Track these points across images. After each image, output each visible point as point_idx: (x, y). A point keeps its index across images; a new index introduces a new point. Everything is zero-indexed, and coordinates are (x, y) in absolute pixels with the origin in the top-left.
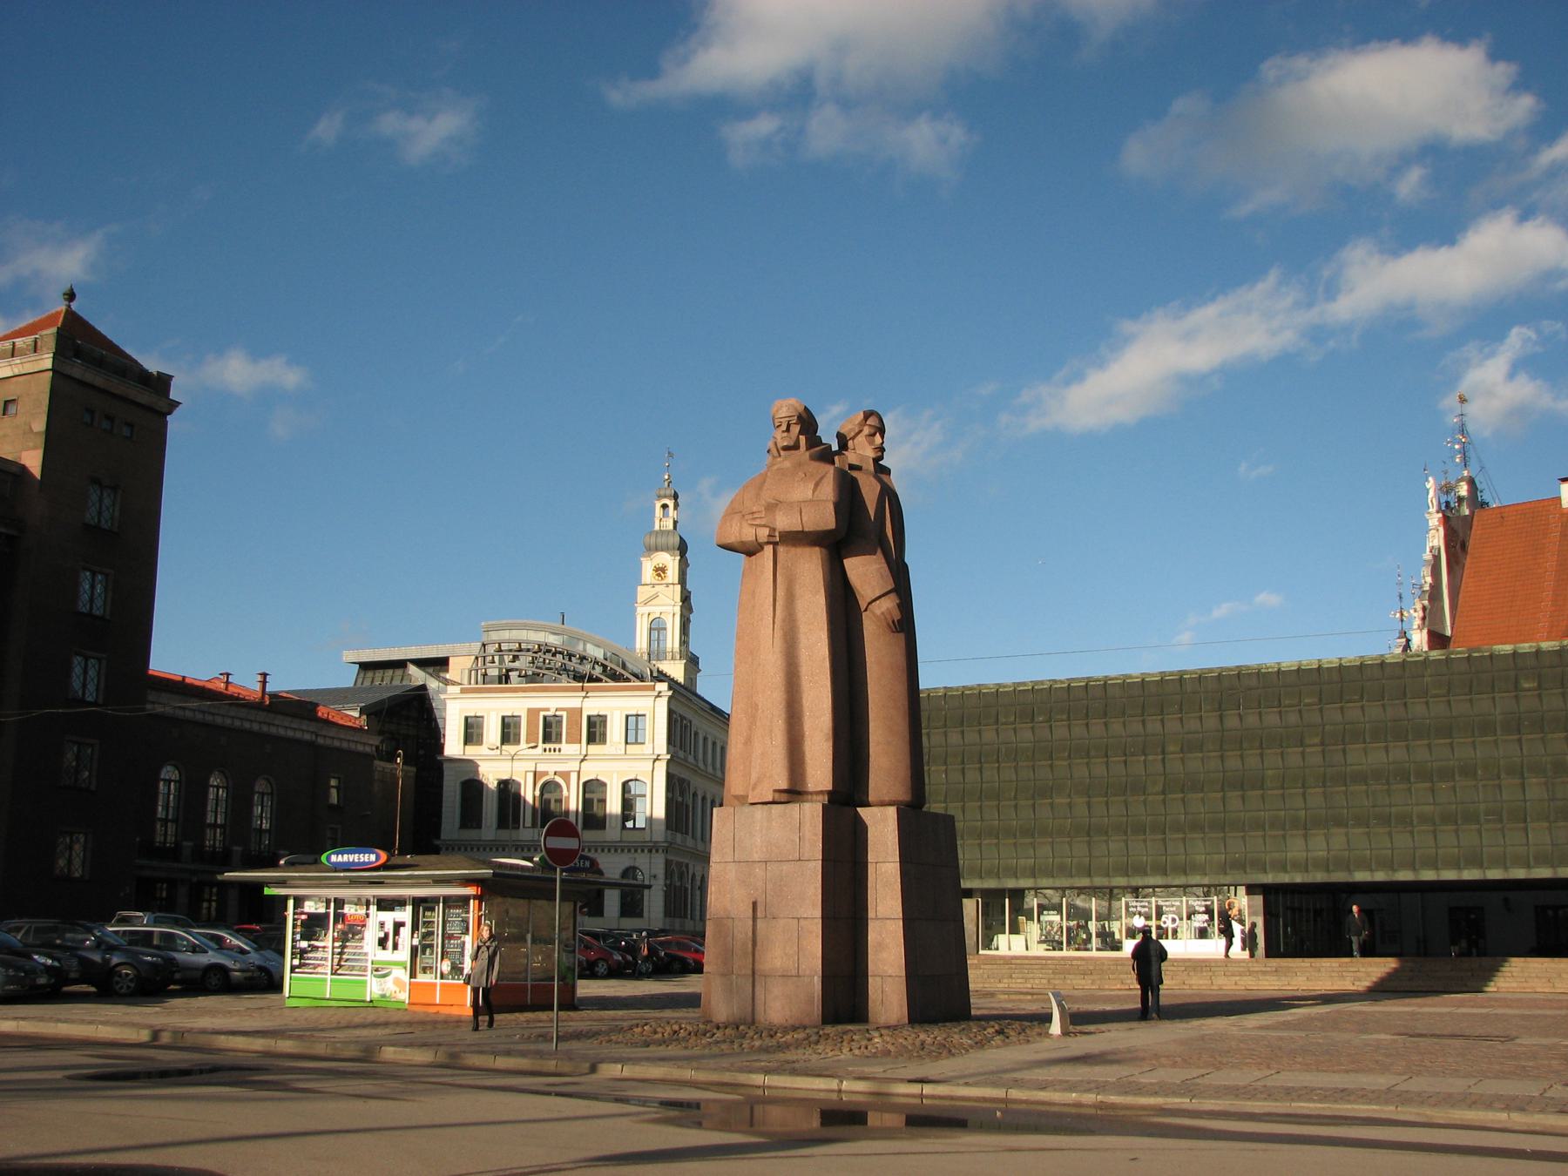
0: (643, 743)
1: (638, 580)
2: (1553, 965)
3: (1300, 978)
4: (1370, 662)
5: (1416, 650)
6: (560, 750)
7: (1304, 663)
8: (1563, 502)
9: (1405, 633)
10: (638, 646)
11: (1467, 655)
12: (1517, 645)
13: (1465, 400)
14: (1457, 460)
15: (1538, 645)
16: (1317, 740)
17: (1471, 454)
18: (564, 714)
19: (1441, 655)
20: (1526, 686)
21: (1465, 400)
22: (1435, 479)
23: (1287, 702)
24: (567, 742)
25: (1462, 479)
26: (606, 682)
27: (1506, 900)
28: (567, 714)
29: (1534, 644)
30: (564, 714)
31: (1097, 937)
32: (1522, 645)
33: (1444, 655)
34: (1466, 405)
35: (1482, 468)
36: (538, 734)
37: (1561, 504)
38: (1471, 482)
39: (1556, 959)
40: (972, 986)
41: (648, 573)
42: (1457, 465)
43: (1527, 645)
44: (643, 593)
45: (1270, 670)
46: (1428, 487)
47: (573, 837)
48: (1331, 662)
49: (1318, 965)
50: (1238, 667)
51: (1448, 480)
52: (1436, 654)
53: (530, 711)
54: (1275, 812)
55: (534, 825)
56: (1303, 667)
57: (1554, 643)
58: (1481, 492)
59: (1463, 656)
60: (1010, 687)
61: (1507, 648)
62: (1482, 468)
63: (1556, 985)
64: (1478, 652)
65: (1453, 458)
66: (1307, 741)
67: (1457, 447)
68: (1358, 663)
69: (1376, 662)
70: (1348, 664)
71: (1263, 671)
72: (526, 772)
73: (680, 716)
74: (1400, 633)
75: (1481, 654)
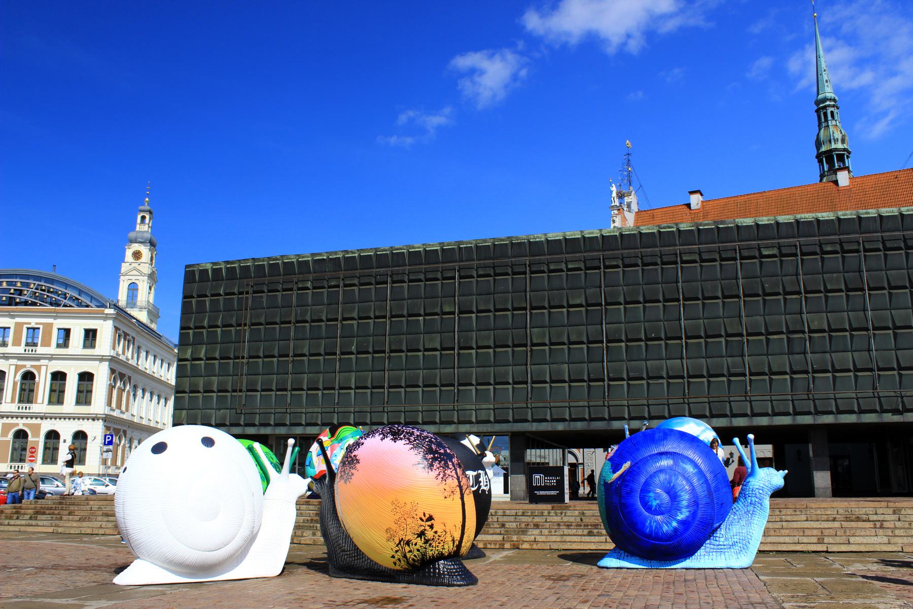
0: (59, 329)
1: (122, 259)
6: (36, 351)
17: (634, 178)
18: (41, 327)
22: (615, 185)
28: (43, 327)
29: (772, 218)
30: (41, 327)
31: (37, 343)
36: (21, 340)
40: (816, 486)
41: (129, 254)
43: (765, 218)
44: (125, 267)
45: (537, 240)
46: (612, 190)
50: (508, 237)
53: (17, 324)
55: (13, 401)
57: (788, 217)
60: (308, 257)
70: (608, 234)
72: (10, 365)
73: (123, 332)
75: (726, 226)
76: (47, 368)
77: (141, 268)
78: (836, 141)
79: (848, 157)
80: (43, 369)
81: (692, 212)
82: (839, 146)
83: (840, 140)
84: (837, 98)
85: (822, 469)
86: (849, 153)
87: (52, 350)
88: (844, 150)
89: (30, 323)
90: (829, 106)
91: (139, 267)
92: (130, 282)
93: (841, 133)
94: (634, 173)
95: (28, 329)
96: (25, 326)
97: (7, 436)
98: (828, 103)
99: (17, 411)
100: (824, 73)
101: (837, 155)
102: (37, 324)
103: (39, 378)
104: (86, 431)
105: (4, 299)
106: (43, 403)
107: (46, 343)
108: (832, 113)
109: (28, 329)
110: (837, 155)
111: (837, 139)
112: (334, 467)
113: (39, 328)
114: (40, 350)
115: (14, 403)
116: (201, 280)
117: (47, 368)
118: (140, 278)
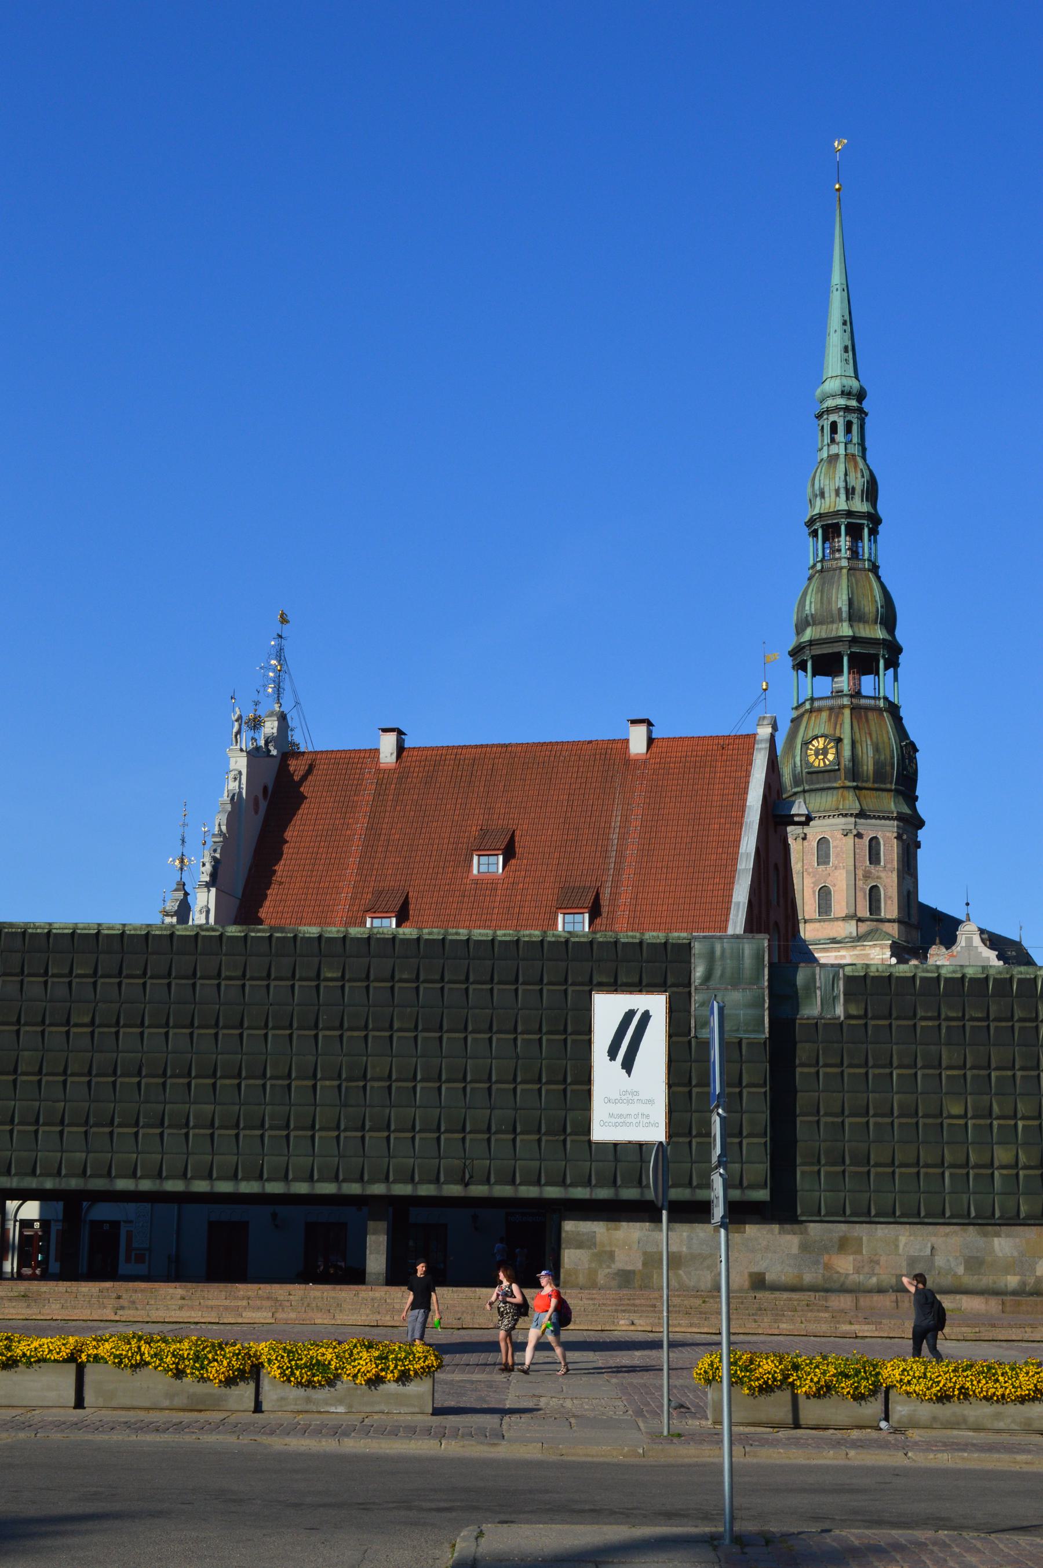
2: (332, 1294)
3: (53, 1306)
4: (157, 933)
5: (899, 1422)
7: (80, 926)
8: (381, 756)
9: (184, 884)
10: (383, 1239)
11: (268, 934)
12: (324, 929)
13: (287, 622)
14: (270, 690)
15: (347, 930)
16: (87, 1020)
17: (286, 685)
19: (240, 932)
20: (329, 975)
21: (287, 622)
23: (56, 971)
25: (271, 715)
27: (274, 1216)
32: (329, 929)
33: (243, 932)
34: (286, 627)
35: (297, 703)
37: (378, 758)
38: (282, 718)
39: (338, 1287)
42: (268, 696)
43: (334, 929)
45: (39, 931)
47: (516, 1343)
48: (112, 928)
49: (74, 1289)
51: (258, 713)
52: (233, 930)
54: (30, 1103)
56: (79, 931)
58: (292, 730)
59: (264, 935)
61: (313, 931)
62: (297, 703)
63: (337, 1317)
64: (282, 932)
65: (265, 686)
66: (74, 1020)
67: (271, 674)
68: (144, 932)
69: (165, 933)
70: (132, 932)
71: (30, 931)
74: (178, 884)
75: (283, 935)
111: (853, 489)
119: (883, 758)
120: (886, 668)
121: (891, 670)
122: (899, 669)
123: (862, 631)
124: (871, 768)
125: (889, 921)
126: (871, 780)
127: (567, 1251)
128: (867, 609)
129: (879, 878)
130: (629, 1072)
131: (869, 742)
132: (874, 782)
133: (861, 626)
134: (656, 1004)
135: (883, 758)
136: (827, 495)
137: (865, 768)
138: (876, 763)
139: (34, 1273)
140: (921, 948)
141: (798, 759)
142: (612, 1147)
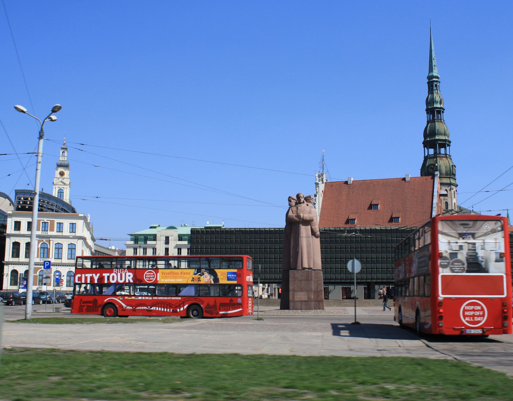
17: (325, 167)
18: (49, 222)
24: (50, 231)
26: (61, 212)
30: (49, 222)
35: (328, 171)
55: (38, 257)
76: (53, 242)
77: (65, 181)
78: (437, 102)
79: (443, 112)
80: (51, 242)
81: (348, 185)
82: (438, 106)
83: (439, 102)
84: (439, 76)
85: (237, 282)
86: (444, 110)
87: (55, 233)
88: (441, 108)
89: (44, 220)
90: (435, 81)
91: (63, 181)
92: (59, 188)
93: (440, 98)
94: (325, 164)
95: (42, 222)
96: (41, 221)
97: (37, 273)
98: (434, 79)
99: (40, 262)
100: (433, 61)
101: (437, 111)
102: (47, 220)
103: (50, 246)
104: (17, 270)
105: (27, 207)
106: (52, 258)
107: (52, 230)
108: (436, 85)
109: (42, 222)
110: (437, 111)
111: (438, 102)
112: (81, 290)
113: (48, 223)
114: (50, 233)
115: (38, 258)
116: (206, 234)
117: (53, 242)
118: (64, 186)
119: (447, 169)
120: (447, 146)
121: (449, 147)
122: (424, 156)
123: (441, 137)
124: (444, 172)
125: (70, 278)
126: (445, 175)
127: (74, 263)
128: (442, 132)
129: (447, 199)
130: (150, 228)
131: (444, 166)
132: (445, 176)
133: (441, 136)
134: (114, 269)
135: (447, 169)
136: (431, 103)
137: (443, 172)
138: (446, 171)
139: (96, 267)
140: (119, 269)
141: (426, 170)
142: (322, 254)
